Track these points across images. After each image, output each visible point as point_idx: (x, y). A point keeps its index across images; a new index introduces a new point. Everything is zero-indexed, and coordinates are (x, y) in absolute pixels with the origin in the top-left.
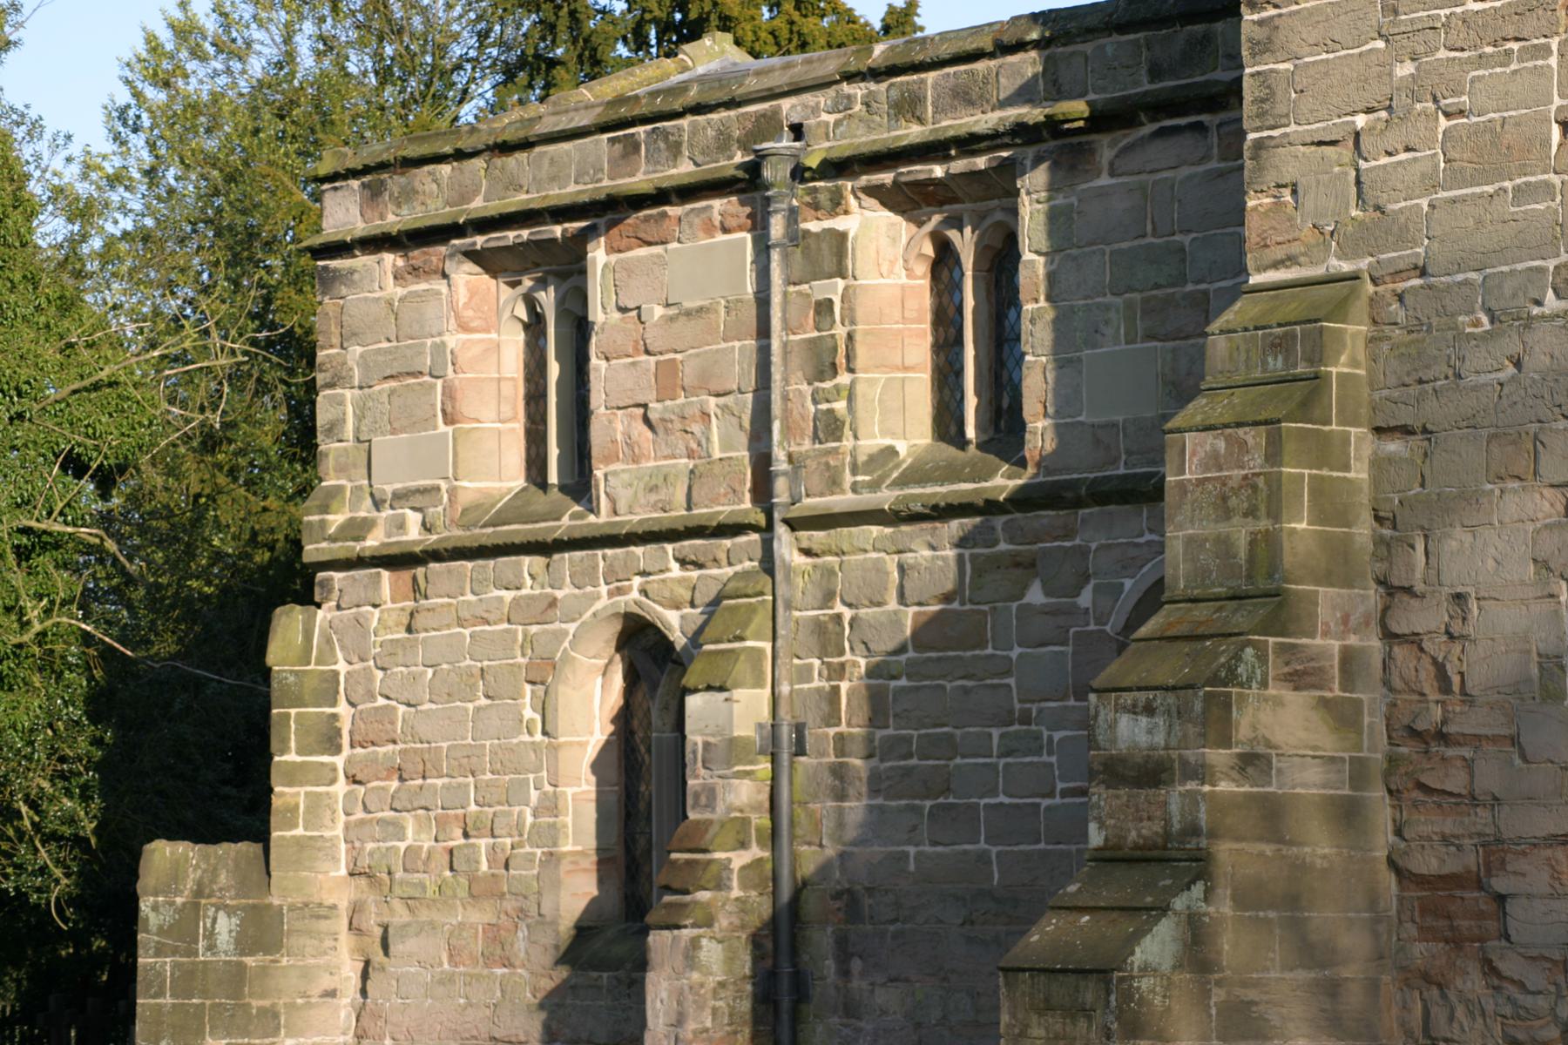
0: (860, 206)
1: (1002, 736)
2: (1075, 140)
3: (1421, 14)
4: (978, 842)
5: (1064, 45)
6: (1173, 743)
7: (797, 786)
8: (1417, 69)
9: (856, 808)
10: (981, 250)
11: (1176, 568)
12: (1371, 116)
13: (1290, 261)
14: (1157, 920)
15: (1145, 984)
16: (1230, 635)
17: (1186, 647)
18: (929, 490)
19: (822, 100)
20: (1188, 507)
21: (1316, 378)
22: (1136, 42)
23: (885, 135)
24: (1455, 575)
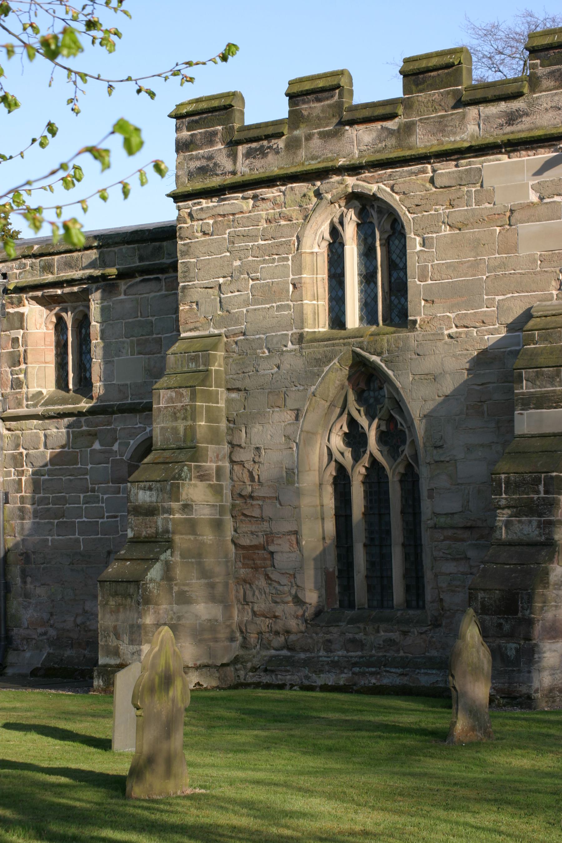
0: (29, 303)
1: (84, 497)
2: (111, 282)
3: (242, 244)
4: (75, 535)
5: (107, 248)
6: (159, 501)
7: (6, 515)
8: (241, 263)
9: (28, 523)
10: (74, 320)
11: (157, 438)
12: (225, 279)
13: (196, 329)
14: (155, 563)
15: (151, 586)
16: (179, 462)
17: (162, 466)
18: (56, 407)
19: (14, 265)
20: (161, 416)
21: (207, 371)
22: (134, 248)
23: (39, 278)
24: (256, 441)
